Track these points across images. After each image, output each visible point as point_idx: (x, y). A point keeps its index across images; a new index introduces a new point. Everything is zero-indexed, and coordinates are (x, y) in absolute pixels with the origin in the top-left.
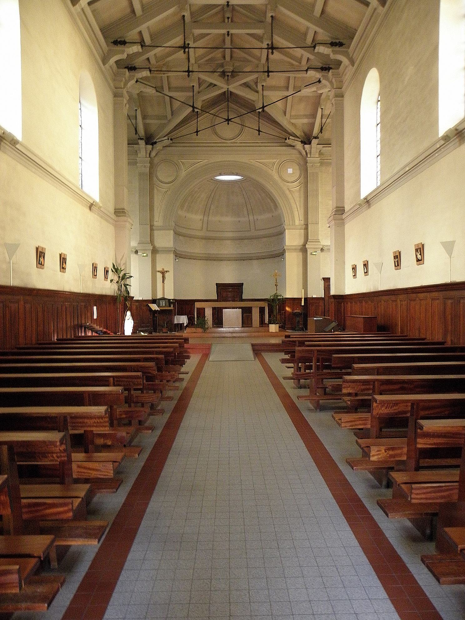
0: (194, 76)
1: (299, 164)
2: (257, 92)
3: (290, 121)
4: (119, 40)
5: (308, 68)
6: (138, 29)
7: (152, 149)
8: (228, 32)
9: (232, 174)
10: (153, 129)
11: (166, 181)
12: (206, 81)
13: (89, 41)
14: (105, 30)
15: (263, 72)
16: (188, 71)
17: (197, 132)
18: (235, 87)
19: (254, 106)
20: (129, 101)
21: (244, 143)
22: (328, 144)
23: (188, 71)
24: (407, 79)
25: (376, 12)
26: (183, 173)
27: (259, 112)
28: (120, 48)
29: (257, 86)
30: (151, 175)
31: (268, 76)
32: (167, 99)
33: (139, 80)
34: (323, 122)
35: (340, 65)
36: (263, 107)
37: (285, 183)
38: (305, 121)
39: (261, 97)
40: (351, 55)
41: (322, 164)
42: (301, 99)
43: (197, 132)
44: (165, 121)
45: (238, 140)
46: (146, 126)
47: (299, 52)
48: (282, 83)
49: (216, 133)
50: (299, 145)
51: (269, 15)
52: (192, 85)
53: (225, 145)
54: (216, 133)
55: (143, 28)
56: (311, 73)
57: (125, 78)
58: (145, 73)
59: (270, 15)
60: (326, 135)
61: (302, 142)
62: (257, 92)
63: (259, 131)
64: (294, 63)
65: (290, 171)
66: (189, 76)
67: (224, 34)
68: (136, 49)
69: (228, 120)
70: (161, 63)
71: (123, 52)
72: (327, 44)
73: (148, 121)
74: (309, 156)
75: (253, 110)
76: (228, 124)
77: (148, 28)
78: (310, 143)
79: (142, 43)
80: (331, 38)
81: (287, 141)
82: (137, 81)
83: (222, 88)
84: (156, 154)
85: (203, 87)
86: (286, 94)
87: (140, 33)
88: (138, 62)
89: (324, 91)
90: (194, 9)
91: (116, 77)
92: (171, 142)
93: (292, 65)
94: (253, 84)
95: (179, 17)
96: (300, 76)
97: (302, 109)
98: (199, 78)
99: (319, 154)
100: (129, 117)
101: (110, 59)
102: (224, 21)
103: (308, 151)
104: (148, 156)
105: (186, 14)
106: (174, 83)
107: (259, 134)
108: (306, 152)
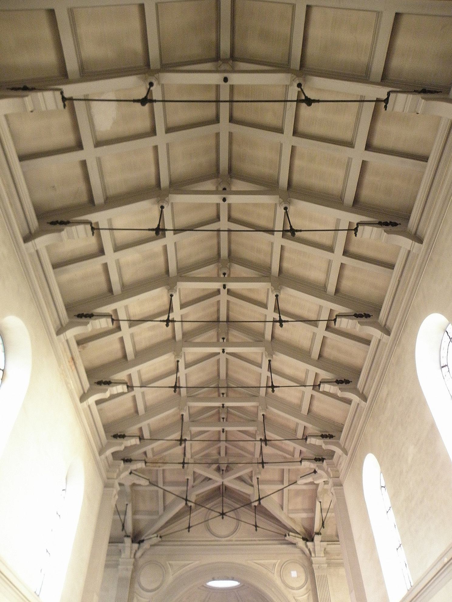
0: (191, 468)
1: (303, 566)
2: (252, 486)
3: (288, 516)
4: (119, 434)
5: (302, 459)
6: (139, 426)
7: (139, 548)
8: (223, 405)
9: (227, 578)
10: (142, 525)
11: (143, 585)
12: (202, 475)
13: (89, 432)
14: (107, 427)
15: (258, 463)
16: (184, 463)
17: (189, 527)
18: (230, 481)
19: (250, 500)
20: (120, 493)
21: (241, 541)
22: (334, 539)
23: (184, 463)
24: (410, 459)
25: (360, 406)
26: (170, 578)
27: (255, 506)
28: (119, 440)
29: (252, 481)
30: (133, 580)
31: (263, 467)
32: (161, 492)
33: (133, 472)
34: (324, 516)
35: (333, 456)
36: (259, 500)
37: (290, 590)
38: (304, 515)
39: (256, 491)
40: (343, 445)
41: (329, 564)
42: (297, 493)
43: (189, 527)
44: (155, 517)
45: (234, 537)
46: (135, 522)
47: (290, 445)
48: (277, 477)
49: (209, 530)
50: (301, 543)
51: (261, 413)
52: (186, 478)
53: (219, 543)
54: (209, 530)
55: (144, 424)
56: (306, 464)
57: (119, 469)
58: (140, 465)
59: (262, 413)
60: (329, 530)
61: (304, 539)
62: (252, 486)
63: (256, 526)
64: (287, 456)
65: (294, 574)
66: (183, 467)
67: (219, 431)
68: (135, 441)
69: (223, 514)
70: (157, 457)
71: (121, 444)
72: (318, 436)
73: (138, 517)
74: (313, 555)
75: (248, 504)
76: (223, 518)
77: (149, 425)
78: (312, 540)
79: (141, 438)
80: (321, 432)
81: (287, 538)
82: (131, 473)
83: (217, 482)
84: (142, 555)
85: (197, 482)
86: (281, 487)
87: (141, 429)
88: (134, 455)
89: (320, 481)
90: (192, 411)
91: (110, 467)
92: (160, 539)
93: (285, 458)
94: (247, 478)
95: (179, 417)
96: (294, 467)
97: (300, 503)
98: (194, 473)
99: (324, 553)
100: (117, 512)
101: (106, 451)
102: (218, 340)
103: (311, 550)
104: (132, 556)
105: (184, 414)
106: (169, 477)
107: (256, 530)
108: (309, 550)
